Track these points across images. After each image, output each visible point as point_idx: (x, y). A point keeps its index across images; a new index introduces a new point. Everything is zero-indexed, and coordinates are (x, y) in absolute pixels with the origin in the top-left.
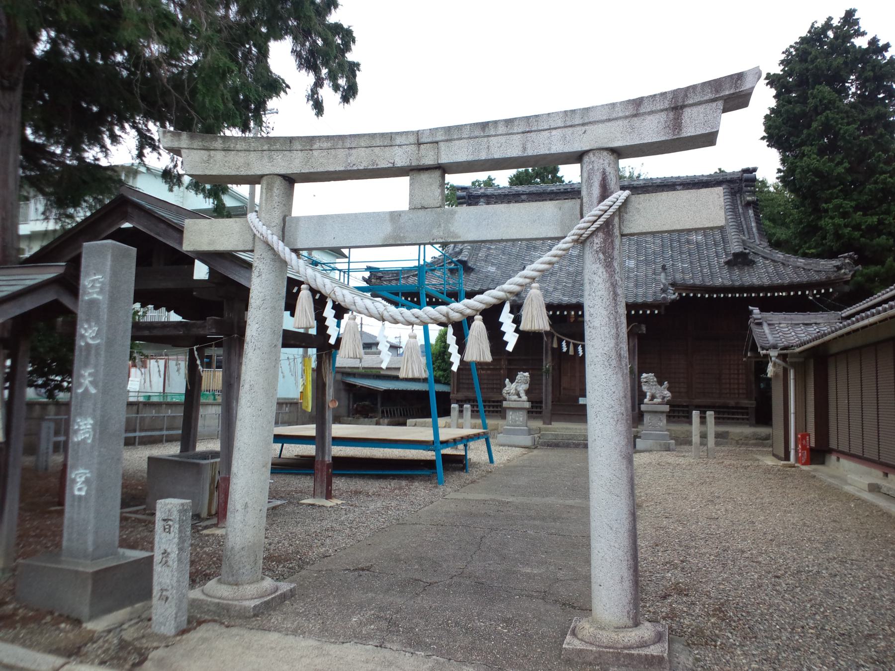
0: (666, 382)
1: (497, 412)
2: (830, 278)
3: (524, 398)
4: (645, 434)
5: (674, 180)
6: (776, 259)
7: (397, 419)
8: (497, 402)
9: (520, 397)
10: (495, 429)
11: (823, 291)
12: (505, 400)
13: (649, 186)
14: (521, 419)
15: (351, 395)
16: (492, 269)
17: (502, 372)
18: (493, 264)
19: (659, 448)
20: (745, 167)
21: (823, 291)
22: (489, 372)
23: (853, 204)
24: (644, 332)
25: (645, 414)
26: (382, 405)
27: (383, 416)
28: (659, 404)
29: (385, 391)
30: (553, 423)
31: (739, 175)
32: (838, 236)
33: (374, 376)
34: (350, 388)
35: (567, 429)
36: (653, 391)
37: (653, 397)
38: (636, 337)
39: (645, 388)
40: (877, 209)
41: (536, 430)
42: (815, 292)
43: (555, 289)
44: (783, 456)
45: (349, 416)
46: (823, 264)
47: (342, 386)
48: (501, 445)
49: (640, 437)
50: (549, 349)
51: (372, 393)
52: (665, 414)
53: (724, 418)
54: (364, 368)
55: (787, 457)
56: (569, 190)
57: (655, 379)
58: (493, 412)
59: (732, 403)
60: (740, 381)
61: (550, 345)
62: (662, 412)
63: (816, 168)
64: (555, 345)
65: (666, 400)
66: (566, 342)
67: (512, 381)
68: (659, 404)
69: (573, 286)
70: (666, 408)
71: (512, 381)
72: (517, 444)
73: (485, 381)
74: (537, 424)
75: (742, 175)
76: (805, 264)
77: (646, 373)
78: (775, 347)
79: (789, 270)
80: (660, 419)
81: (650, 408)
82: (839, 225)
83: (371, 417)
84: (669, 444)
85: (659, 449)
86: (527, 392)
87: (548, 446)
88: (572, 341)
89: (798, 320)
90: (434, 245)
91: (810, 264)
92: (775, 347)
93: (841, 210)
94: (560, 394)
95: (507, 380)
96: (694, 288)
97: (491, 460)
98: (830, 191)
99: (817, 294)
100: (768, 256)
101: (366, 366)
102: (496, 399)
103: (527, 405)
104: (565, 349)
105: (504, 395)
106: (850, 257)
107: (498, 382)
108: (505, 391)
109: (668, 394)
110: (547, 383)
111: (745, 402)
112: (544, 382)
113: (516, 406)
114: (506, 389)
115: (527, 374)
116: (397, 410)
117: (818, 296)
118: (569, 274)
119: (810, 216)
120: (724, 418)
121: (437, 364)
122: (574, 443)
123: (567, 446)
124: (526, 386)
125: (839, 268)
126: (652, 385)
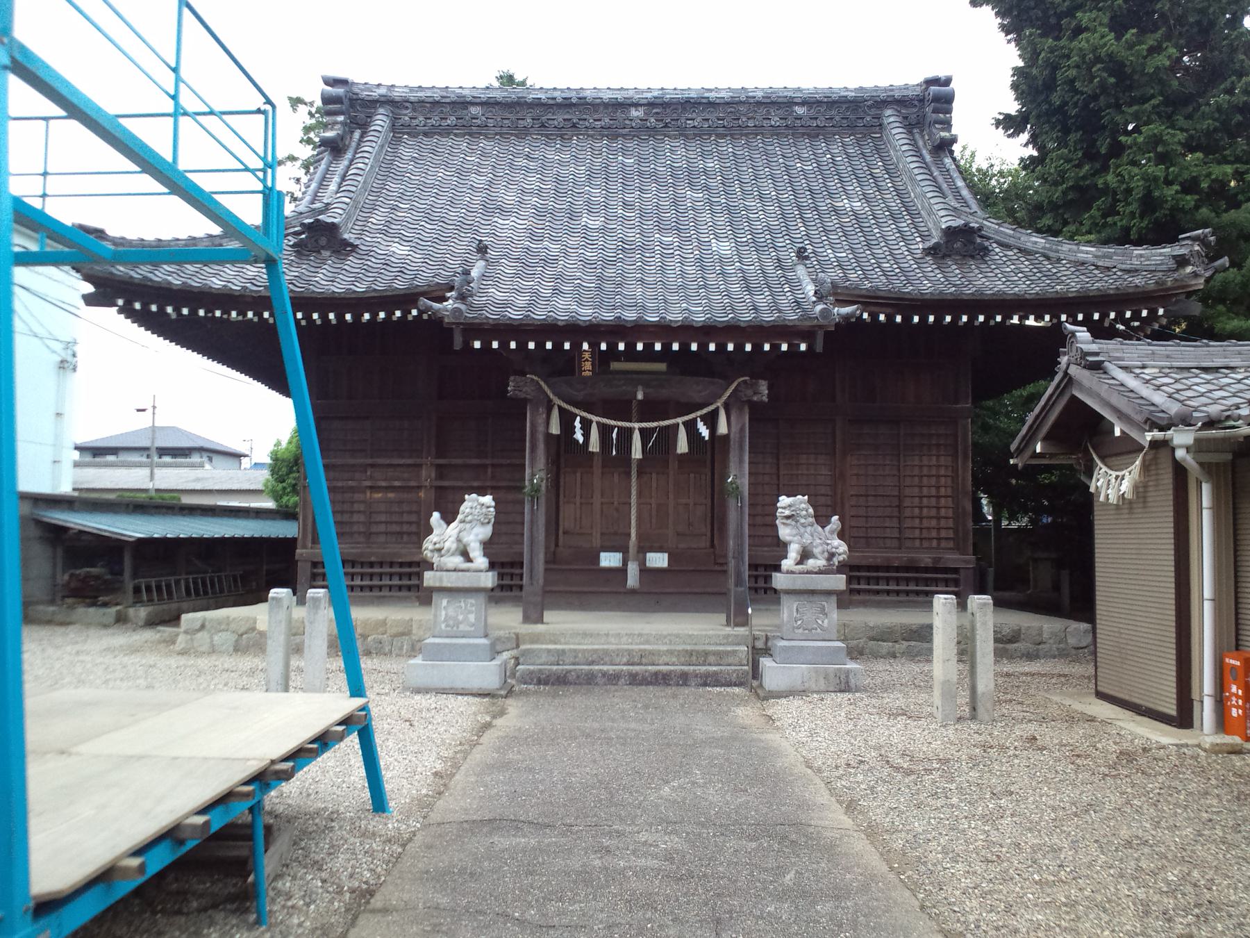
0: (835, 518)
1: (409, 588)
2: (1164, 283)
3: (481, 561)
4: (785, 649)
5: (789, 94)
6: (1029, 246)
7: (165, 607)
8: (410, 564)
9: (468, 559)
10: (403, 634)
11: (1144, 313)
12: (430, 567)
13: (741, 102)
14: (472, 618)
15: (60, 552)
16: (400, 249)
17: (422, 494)
18: (403, 239)
19: (822, 684)
20: (931, 74)
21: (1144, 313)
22: (391, 495)
23: (1181, 136)
24: (765, 399)
25: (784, 598)
26: (135, 575)
27: (138, 601)
28: (820, 572)
29: (140, 541)
30: (548, 616)
31: (918, 91)
32: (1149, 203)
33: (128, 505)
34: (57, 534)
35: (585, 635)
36: (807, 539)
37: (805, 555)
38: (747, 410)
39: (784, 532)
40: (1227, 152)
41: (508, 639)
42: (1128, 314)
43: (556, 291)
44: (1172, 710)
45: (52, 602)
46: (1141, 256)
47: (34, 532)
48: (418, 691)
49: (767, 651)
50: (541, 437)
51: (110, 548)
52: (834, 598)
53: (907, 593)
54: (158, 490)
55: (1184, 718)
56: (574, 101)
57: (811, 510)
58: (400, 588)
59: (926, 559)
60: (943, 512)
61: (541, 429)
62: (828, 593)
63: (1110, 56)
64: (555, 429)
65: (835, 561)
66: (583, 420)
67: (449, 518)
68: (820, 572)
69: (599, 288)
70: (839, 582)
71: (449, 518)
72: (459, 684)
73: (383, 518)
74: (508, 619)
75: (926, 89)
76: (1096, 257)
77: (788, 496)
78: (1185, 420)
79: (1065, 271)
80: (823, 611)
81: (801, 582)
82: (1156, 179)
83: (105, 605)
84: (848, 672)
85: (822, 687)
86: (487, 546)
87: (539, 682)
88: (595, 419)
89: (1183, 360)
90: (207, 110)
91: (1104, 256)
92: (1185, 420)
93: (1160, 149)
94: (557, 545)
95: (436, 515)
96: (871, 300)
97: (379, 803)
98: (1135, 108)
99: (1132, 319)
100: (1011, 241)
101: (163, 487)
102: (408, 559)
103: (489, 580)
104: (579, 436)
105: (428, 554)
106: (1202, 241)
107: (413, 518)
108: (428, 544)
109: (841, 547)
110: (535, 519)
111: (953, 558)
112: (527, 517)
113: (460, 585)
114: (433, 538)
115: (488, 500)
116: (177, 582)
117: (1136, 324)
118: (586, 262)
119: (1079, 166)
120: (907, 593)
121: (290, 481)
122: (604, 674)
123: (589, 680)
124: (486, 532)
125: (1181, 261)
126: (804, 525)
